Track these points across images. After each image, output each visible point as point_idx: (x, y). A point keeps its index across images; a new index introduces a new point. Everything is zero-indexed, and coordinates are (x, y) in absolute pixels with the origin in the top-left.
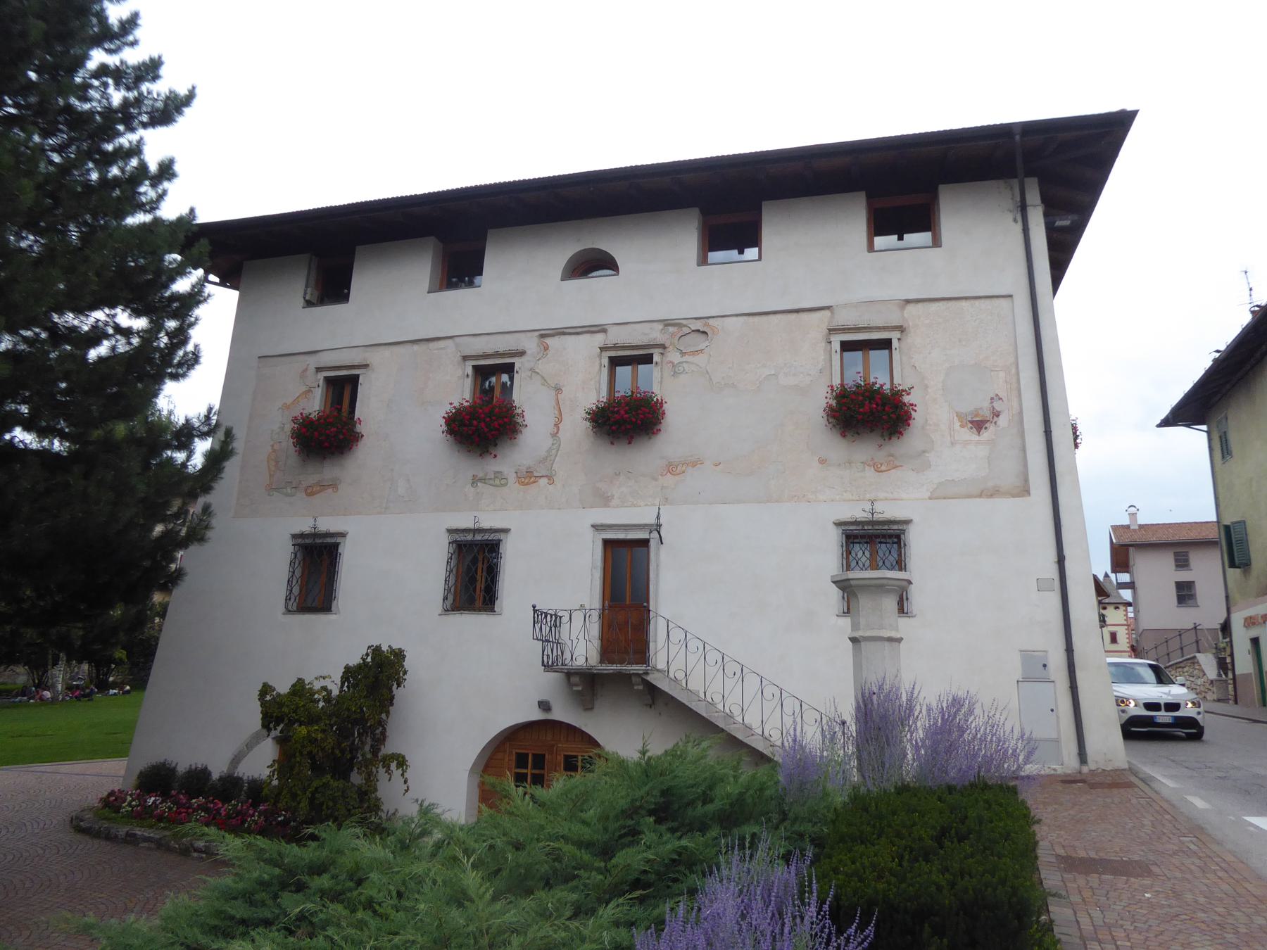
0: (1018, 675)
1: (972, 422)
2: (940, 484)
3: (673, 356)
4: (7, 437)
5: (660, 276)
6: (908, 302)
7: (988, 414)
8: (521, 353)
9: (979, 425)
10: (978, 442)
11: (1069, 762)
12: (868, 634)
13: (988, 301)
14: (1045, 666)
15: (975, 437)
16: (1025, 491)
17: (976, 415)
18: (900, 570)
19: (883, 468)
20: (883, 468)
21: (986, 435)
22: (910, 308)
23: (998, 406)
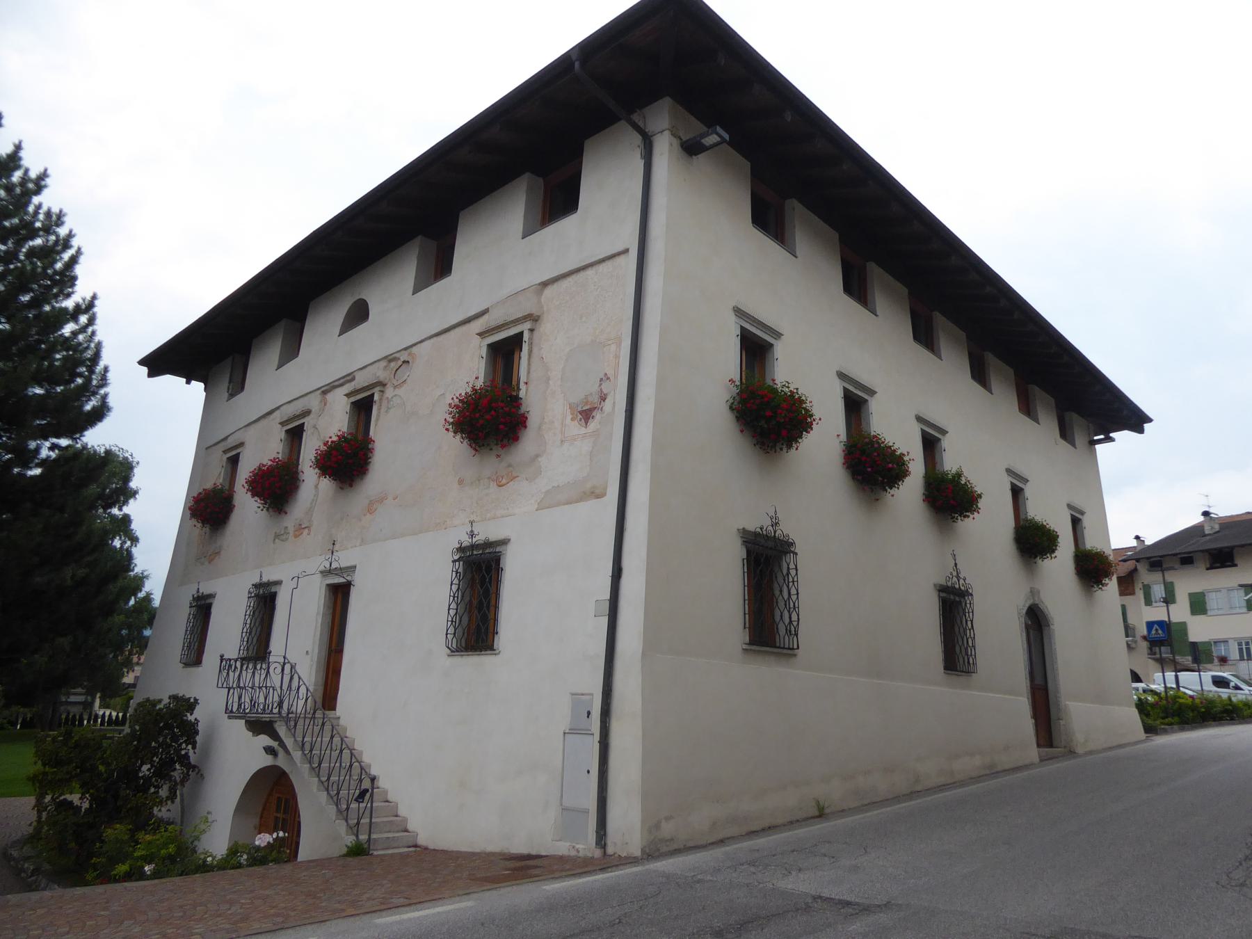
0: (565, 725)
1: (581, 413)
2: (547, 492)
3: (389, 392)
4: (32, 445)
5: (501, 257)
6: (545, 284)
7: (596, 399)
8: (307, 413)
9: (586, 415)
10: (584, 436)
11: (586, 845)
12: (801, 832)
13: (609, 264)
14: (589, 713)
15: (583, 431)
16: (597, 494)
17: (586, 403)
18: (1051, 746)
19: (504, 481)
20: (504, 481)
21: (593, 425)
22: (548, 291)
23: (606, 387)
